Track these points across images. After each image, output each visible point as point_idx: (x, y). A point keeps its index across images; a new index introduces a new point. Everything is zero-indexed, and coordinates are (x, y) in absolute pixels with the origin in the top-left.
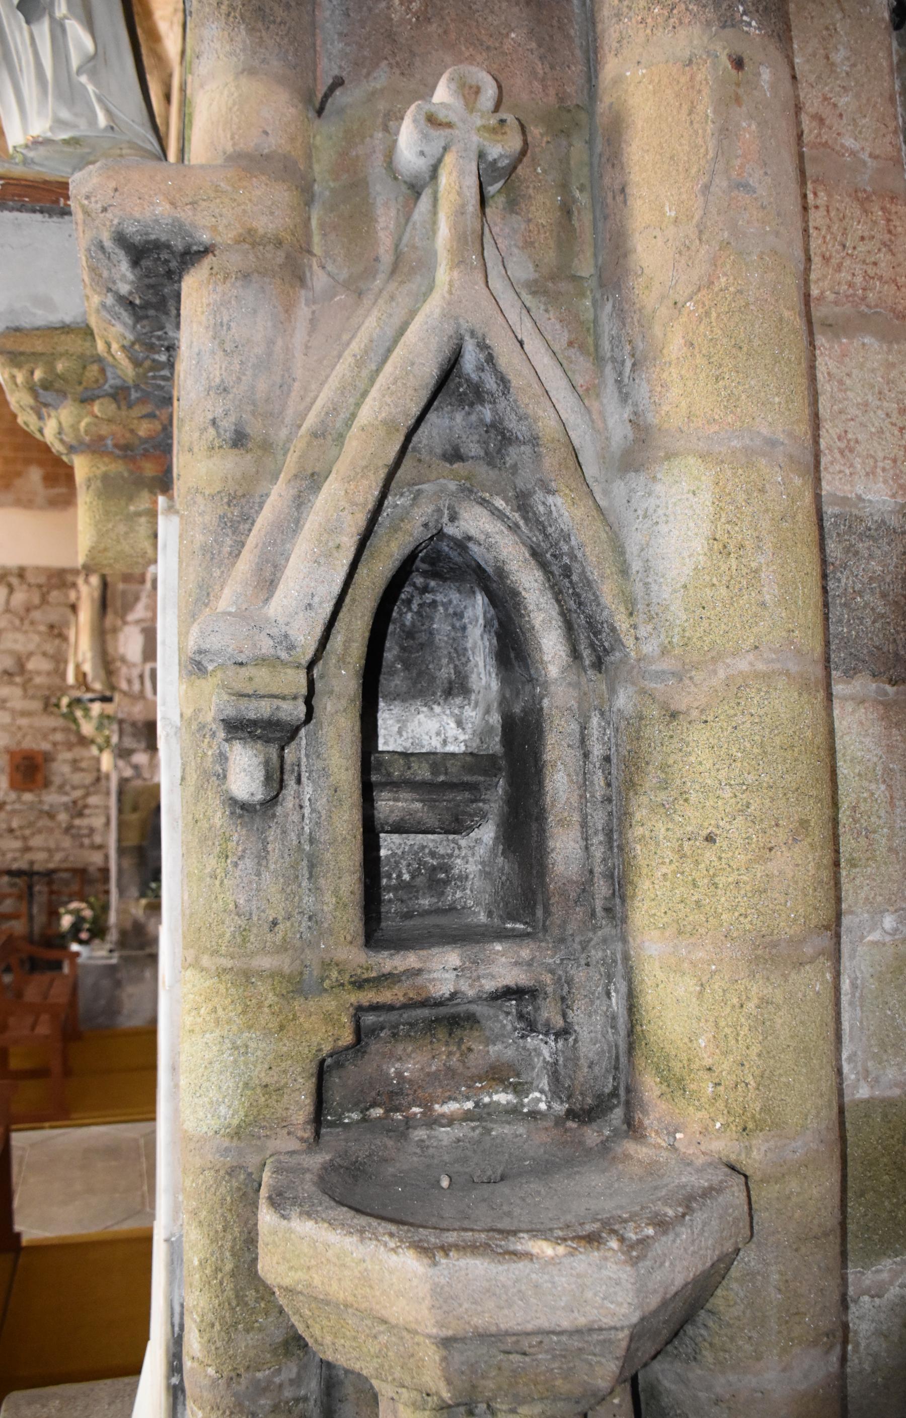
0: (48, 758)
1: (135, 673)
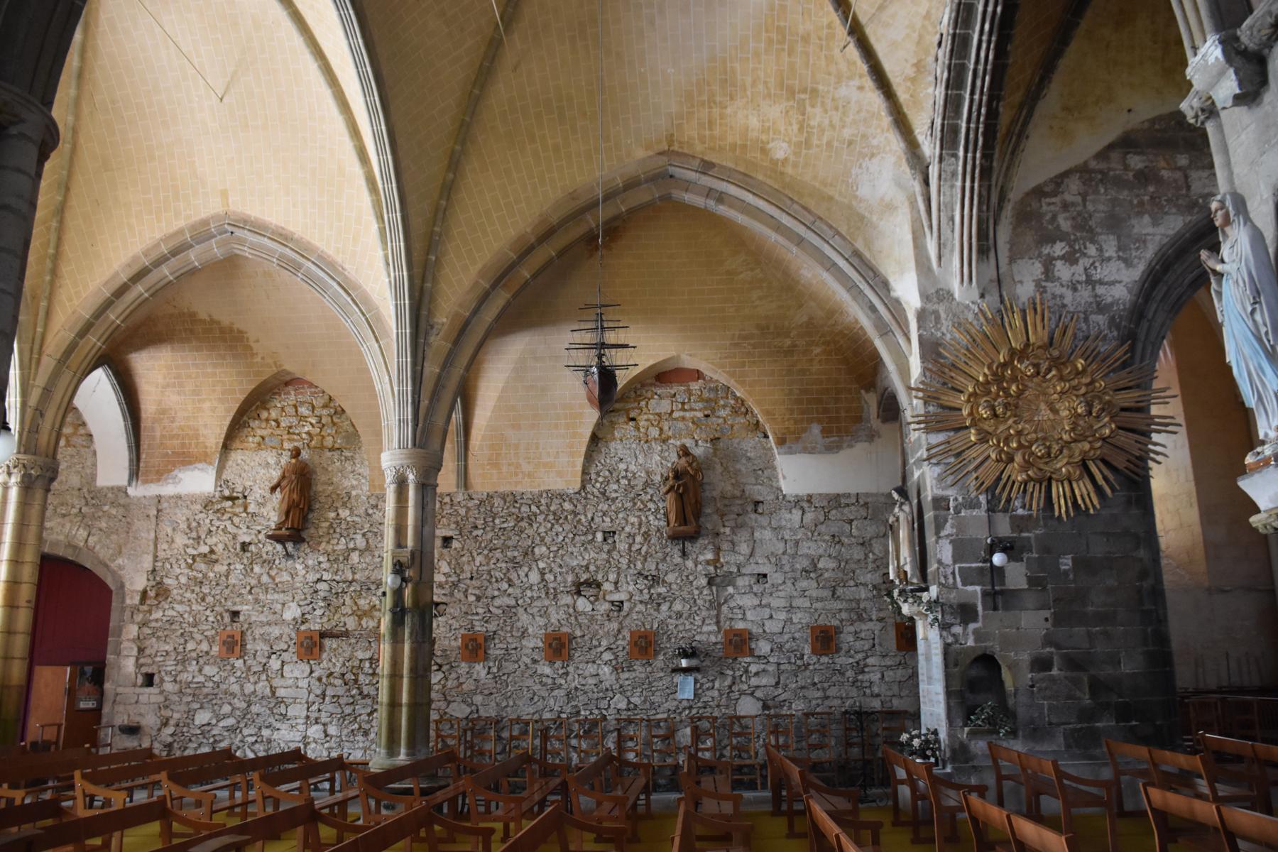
0: (838, 631)
1: (949, 571)
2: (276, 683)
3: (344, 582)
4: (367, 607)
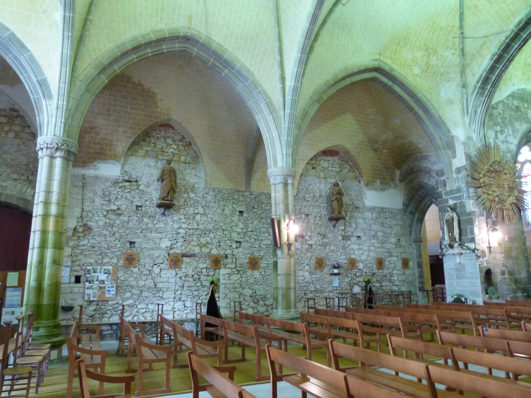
2: (157, 280)
3: (193, 229)
4: (205, 242)
